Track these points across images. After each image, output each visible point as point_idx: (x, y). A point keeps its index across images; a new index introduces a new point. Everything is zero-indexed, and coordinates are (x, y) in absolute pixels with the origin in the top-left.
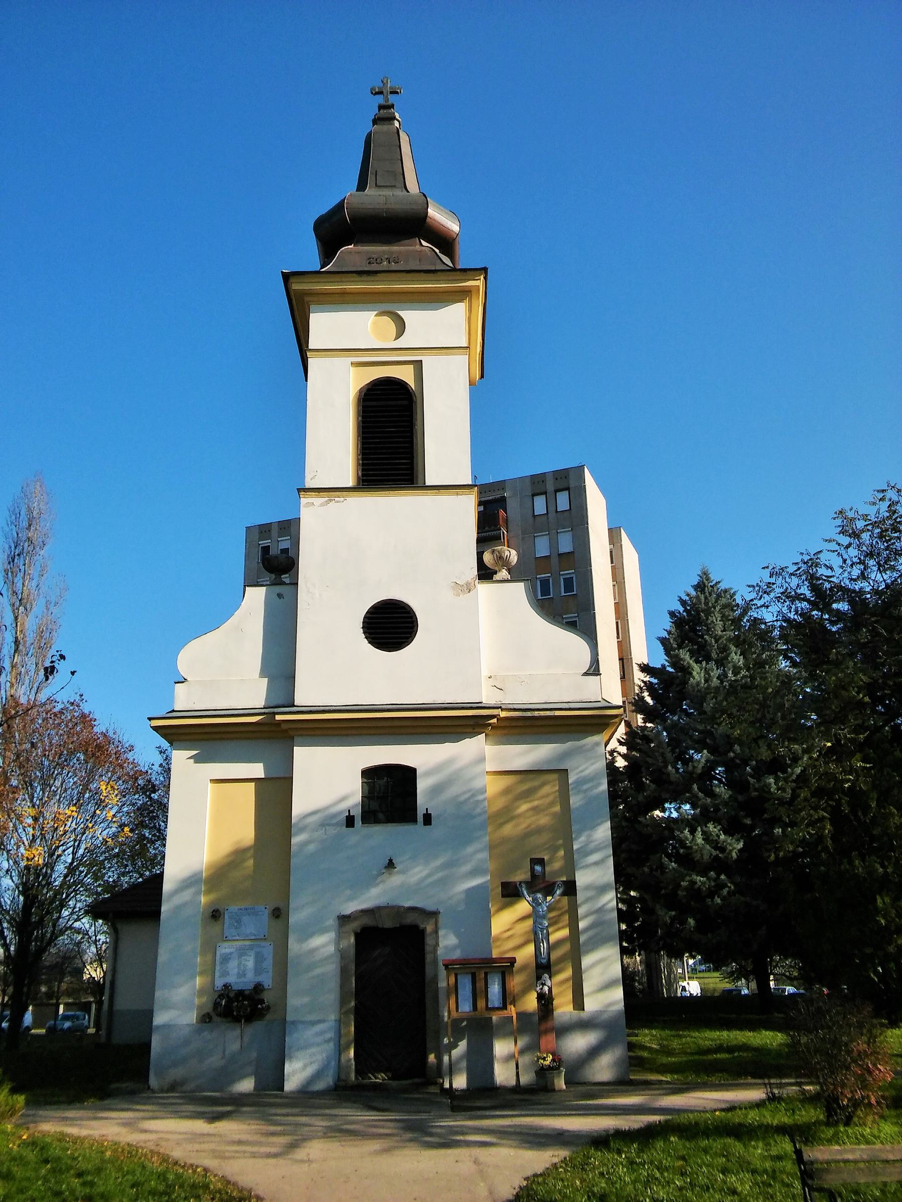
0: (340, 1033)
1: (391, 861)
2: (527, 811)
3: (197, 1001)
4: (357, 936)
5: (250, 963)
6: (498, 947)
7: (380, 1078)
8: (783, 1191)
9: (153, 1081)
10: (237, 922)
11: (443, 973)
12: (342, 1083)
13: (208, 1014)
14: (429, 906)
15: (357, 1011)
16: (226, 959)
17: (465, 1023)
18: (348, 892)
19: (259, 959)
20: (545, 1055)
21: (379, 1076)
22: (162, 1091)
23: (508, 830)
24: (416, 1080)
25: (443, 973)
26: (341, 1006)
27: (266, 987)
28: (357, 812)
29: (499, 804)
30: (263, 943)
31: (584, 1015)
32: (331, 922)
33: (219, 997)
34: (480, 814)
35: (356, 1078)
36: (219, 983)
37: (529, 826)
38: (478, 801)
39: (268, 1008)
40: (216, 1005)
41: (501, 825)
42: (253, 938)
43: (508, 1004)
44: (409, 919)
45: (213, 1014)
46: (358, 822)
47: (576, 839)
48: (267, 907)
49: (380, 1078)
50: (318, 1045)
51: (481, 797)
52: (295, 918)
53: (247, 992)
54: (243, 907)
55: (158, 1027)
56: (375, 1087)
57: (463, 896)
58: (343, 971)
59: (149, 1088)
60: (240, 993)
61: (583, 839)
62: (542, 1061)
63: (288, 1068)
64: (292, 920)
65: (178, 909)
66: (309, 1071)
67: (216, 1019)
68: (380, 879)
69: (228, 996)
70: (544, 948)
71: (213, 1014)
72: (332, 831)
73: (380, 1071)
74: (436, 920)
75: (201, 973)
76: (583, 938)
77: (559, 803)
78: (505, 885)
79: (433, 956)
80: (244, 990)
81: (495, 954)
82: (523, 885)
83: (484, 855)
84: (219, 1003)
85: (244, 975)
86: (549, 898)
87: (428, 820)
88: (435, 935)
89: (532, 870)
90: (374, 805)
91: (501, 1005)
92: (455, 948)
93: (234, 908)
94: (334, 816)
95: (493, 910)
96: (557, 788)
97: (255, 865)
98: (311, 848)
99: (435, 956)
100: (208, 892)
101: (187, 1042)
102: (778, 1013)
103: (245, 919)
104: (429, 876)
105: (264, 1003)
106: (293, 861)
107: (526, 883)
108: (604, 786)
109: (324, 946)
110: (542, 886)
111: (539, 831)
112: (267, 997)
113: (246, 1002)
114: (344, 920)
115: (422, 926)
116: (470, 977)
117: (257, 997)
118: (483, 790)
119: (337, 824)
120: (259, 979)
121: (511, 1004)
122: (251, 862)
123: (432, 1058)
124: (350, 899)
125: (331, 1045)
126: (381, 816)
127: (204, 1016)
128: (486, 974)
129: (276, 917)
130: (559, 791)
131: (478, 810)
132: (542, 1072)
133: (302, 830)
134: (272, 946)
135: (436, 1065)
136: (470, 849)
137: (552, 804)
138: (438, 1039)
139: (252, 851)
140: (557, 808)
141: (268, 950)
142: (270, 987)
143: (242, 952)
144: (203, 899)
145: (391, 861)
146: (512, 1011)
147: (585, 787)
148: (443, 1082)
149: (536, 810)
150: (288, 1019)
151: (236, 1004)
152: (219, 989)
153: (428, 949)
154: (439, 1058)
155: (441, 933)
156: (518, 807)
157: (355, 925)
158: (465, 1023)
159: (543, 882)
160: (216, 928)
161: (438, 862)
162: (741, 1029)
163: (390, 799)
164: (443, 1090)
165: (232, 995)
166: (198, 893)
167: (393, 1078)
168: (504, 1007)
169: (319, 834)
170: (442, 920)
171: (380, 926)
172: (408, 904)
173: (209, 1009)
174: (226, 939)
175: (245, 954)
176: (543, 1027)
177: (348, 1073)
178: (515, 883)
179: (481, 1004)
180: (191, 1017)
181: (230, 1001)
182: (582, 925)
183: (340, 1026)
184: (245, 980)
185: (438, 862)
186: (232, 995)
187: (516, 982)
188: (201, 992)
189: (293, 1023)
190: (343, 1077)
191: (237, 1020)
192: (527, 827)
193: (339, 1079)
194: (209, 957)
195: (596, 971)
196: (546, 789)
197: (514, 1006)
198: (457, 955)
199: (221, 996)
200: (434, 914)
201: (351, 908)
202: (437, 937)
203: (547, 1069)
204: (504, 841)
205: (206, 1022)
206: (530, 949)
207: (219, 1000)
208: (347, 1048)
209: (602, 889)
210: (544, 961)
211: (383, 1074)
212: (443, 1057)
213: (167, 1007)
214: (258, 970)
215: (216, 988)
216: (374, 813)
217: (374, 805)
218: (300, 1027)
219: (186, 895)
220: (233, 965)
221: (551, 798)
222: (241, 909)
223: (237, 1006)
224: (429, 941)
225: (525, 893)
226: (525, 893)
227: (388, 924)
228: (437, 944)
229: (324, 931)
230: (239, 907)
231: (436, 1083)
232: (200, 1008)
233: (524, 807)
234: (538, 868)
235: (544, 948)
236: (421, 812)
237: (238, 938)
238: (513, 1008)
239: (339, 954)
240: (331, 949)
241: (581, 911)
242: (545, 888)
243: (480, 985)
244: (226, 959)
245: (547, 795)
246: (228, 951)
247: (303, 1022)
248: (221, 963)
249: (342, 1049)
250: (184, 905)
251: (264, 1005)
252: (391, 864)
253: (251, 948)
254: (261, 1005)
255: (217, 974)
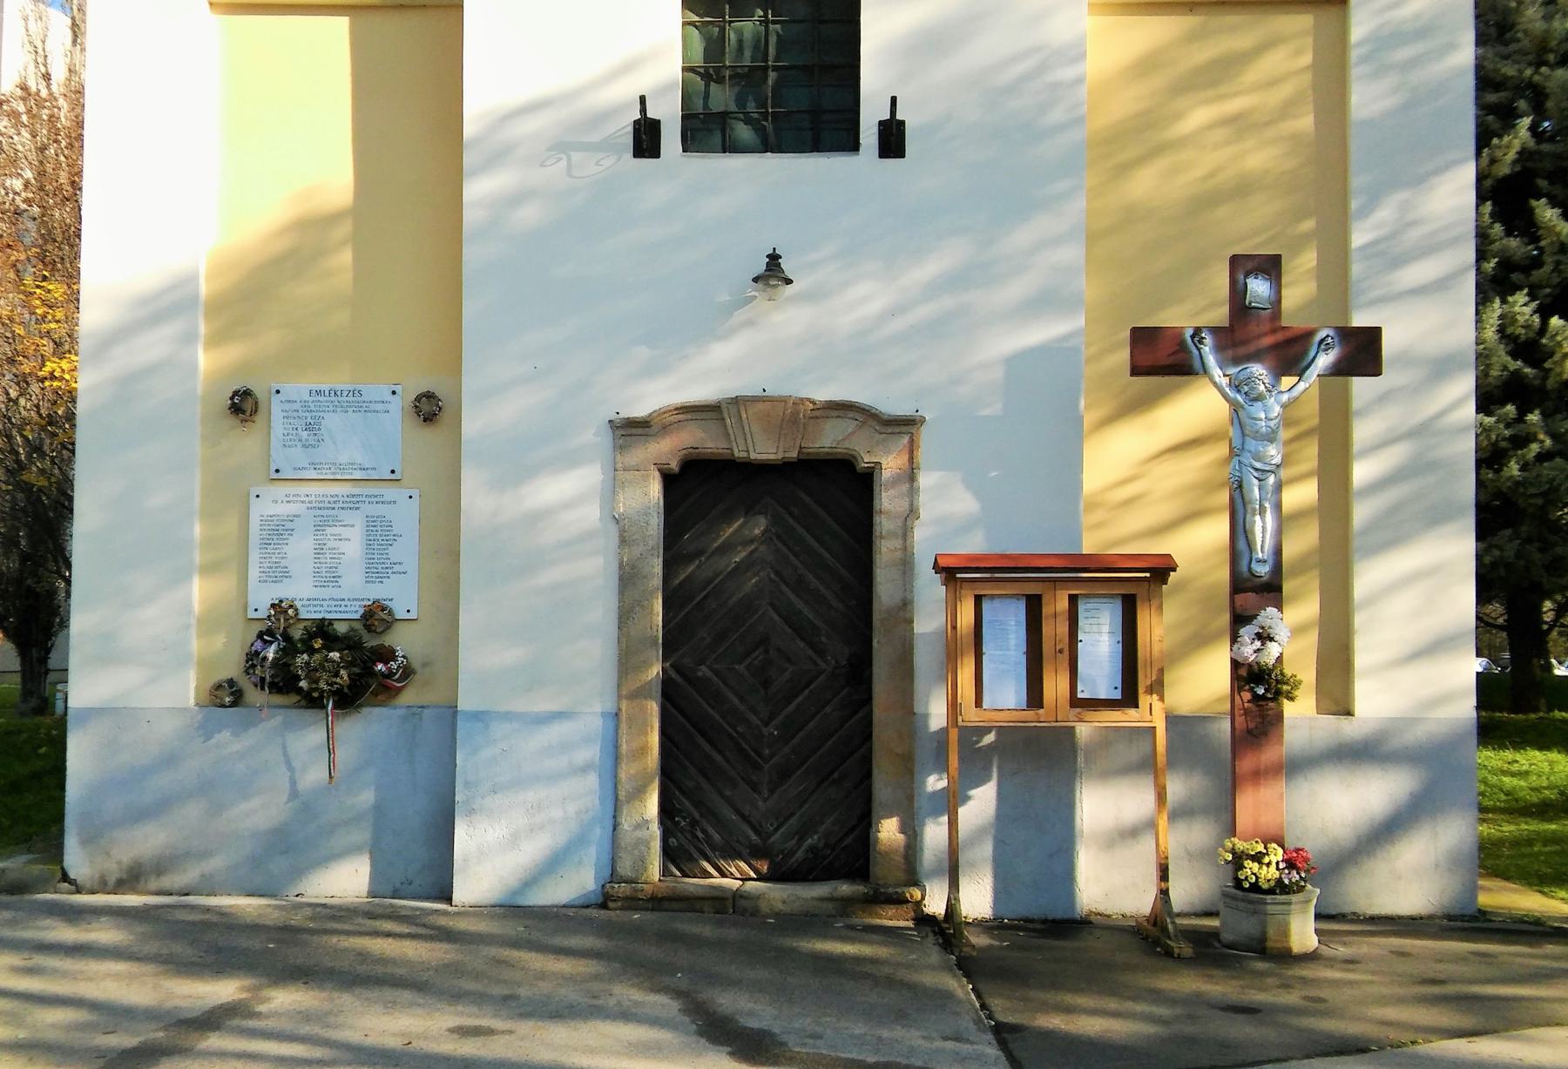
0: (617, 747)
1: (774, 258)
2: (1212, 126)
3: (195, 645)
4: (670, 481)
5: (351, 544)
6: (1099, 526)
7: (734, 877)
8: (828, 709)
9: (76, 859)
10: (308, 427)
11: (930, 591)
12: (622, 889)
13: (231, 682)
14: (892, 404)
15: (670, 694)
16: (279, 531)
17: (990, 738)
18: (643, 352)
19: (379, 536)
20: (1260, 848)
21: (733, 870)
22: (102, 887)
23: (1144, 184)
24: (845, 888)
25: (930, 591)
26: (620, 678)
27: (400, 613)
28: (668, 112)
29: (1125, 103)
30: (389, 492)
31: (1349, 729)
32: (594, 436)
33: (260, 636)
34: (1061, 128)
35: (665, 872)
36: (261, 599)
37: (1211, 175)
38: (1056, 86)
39: (407, 672)
40: (253, 659)
41: (1125, 169)
42: (358, 475)
43: (1141, 690)
44: (829, 439)
45: (245, 684)
46: (671, 138)
47: (1366, 211)
48: (398, 389)
49: (734, 877)
50: (553, 778)
51: (1067, 73)
52: (475, 421)
53: (341, 628)
54: (325, 387)
55: (90, 713)
56: (725, 905)
57: (998, 373)
58: (628, 578)
59: (65, 877)
60: (322, 629)
61: (1385, 214)
62: (1255, 866)
63: (465, 838)
64: (472, 424)
65: (129, 384)
66: (532, 851)
67: (254, 696)
68: (741, 315)
69: (287, 637)
70: (1264, 528)
71: (245, 684)
72: (594, 167)
73: (732, 854)
74: (912, 441)
75: (208, 569)
76: (1361, 513)
77: (1310, 107)
78: (1143, 338)
79: (898, 543)
80: (331, 622)
81: (1090, 544)
82: (1209, 340)
83: (1072, 254)
84: (257, 653)
85: (335, 579)
86: (1287, 381)
87: (892, 140)
88: (905, 487)
89: (1238, 294)
90: (722, 98)
91: (1117, 695)
92: (968, 526)
93: (297, 388)
94: (601, 117)
95: (1089, 418)
96: (1307, 59)
97: (356, 259)
98: (528, 215)
99: (905, 549)
100: (215, 341)
101: (170, 760)
102: (1560, 710)
103: (333, 422)
104: (893, 312)
105: (394, 658)
106: (472, 255)
107: (1215, 330)
108: (1464, 54)
109: (569, 505)
110: (1267, 341)
111: (1242, 189)
112: (403, 642)
113: (335, 655)
114: (630, 430)
115: (866, 460)
116: (1021, 607)
117: (371, 642)
118: (1075, 53)
119: (604, 146)
120: (376, 592)
121: (1150, 690)
122: (346, 257)
123: (889, 830)
124: (651, 370)
125: (592, 780)
126: (743, 132)
127: (219, 687)
128: (1073, 600)
129: (425, 421)
130: (1315, 67)
131: (1056, 115)
132: (1246, 893)
133: (497, 158)
134: (416, 501)
135: (902, 850)
136: (1023, 236)
137: (1286, 110)
138: (909, 771)
139: (345, 229)
140: (1305, 122)
141: (404, 512)
142: (413, 615)
143: (325, 516)
144: (204, 360)
145: (774, 258)
146: (1151, 713)
147: (1405, 53)
148: (923, 898)
149: (1239, 124)
150: (462, 705)
151: (305, 656)
152: (262, 614)
153: (884, 524)
154: (912, 831)
155: (925, 480)
156: (1179, 116)
157: (668, 449)
158: (990, 738)
159: (1274, 331)
160: (244, 443)
161: (929, 269)
162: (1543, 746)
163: (772, 76)
164: (925, 921)
165: (297, 633)
166: (189, 338)
167: (776, 875)
168: (1129, 698)
169: (555, 172)
170: (927, 438)
171: (739, 454)
172: (823, 394)
173: (232, 668)
174: (277, 477)
175: (336, 521)
176: (1246, 764)
177: (642, 862)
178: (1177, 333)
179: (1055, 686)
180: (186, 689)
181: (290, 648)
182: (1362, 472)
183: (617, 728)
184: (337, 593)
185: (929, 269)
186: (297, 633)
187: (1156, 629)
188: (208, 624)
189: (478, 716)
190: (625, 868)
191: (313, 701)
192: (1205, 178)
193: (614, 877)
194: (230, 526)
195: (1402, 604)
196: (1273, 62)
197: (1162, 699)
198: (973, 544)
199: (266, 636)
200: (906, 425)
201: (648, 400)
202: (913, 492)
203: (1271, 891)
204: (1131, 216)
205: (223, 706)
206: (1216, 531)
207: (259, 645)
208: (639, 793)
209: (1441, 368)
210: (1263, 570)
211: (742, 864)
212: (923, 825)
213: (109, 655)
214: (377, 568)
215: (252, 615)
216: (722, 119)
217: (722, 98)
218: (499, 729)
219: (152, 346)
220: (300, 548)
221: (1286, 90)
222: (318, 393)
223: (307, 664)
224: (888, 501)
225: (1211, 360)
226: (1211, 360)
227: (764, 449)
228: (912, 512)
229: (570, 460)
230: (315, 387)
231: (901, 901)
232: (204, 665)
233: (1198, 116)
234: (1258, 288)
235: (1264, 528)
236: (871, 114)
237: (313, 475)
238: (1157, 705)
239: (613, 531)
240: (592, 514)
241: (1363, 431)
242: (1275, 347)
243: (1055, 630)
244: (279, 531)
245: (1272, 83)
246: (283, 510)
247: (508, 716)
248: (265, 544)
249: (622, 794)
250: (150, 370)
251: (394, 665)
252: (773, 271)
253: (353, 504)
254: (386, 663)
255: (254, 573)
